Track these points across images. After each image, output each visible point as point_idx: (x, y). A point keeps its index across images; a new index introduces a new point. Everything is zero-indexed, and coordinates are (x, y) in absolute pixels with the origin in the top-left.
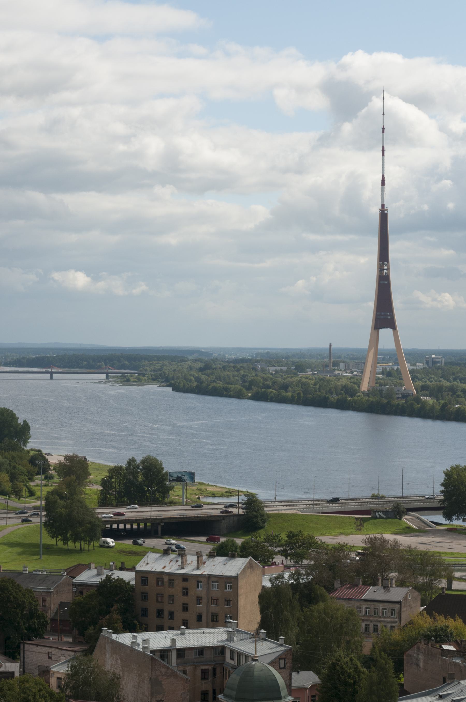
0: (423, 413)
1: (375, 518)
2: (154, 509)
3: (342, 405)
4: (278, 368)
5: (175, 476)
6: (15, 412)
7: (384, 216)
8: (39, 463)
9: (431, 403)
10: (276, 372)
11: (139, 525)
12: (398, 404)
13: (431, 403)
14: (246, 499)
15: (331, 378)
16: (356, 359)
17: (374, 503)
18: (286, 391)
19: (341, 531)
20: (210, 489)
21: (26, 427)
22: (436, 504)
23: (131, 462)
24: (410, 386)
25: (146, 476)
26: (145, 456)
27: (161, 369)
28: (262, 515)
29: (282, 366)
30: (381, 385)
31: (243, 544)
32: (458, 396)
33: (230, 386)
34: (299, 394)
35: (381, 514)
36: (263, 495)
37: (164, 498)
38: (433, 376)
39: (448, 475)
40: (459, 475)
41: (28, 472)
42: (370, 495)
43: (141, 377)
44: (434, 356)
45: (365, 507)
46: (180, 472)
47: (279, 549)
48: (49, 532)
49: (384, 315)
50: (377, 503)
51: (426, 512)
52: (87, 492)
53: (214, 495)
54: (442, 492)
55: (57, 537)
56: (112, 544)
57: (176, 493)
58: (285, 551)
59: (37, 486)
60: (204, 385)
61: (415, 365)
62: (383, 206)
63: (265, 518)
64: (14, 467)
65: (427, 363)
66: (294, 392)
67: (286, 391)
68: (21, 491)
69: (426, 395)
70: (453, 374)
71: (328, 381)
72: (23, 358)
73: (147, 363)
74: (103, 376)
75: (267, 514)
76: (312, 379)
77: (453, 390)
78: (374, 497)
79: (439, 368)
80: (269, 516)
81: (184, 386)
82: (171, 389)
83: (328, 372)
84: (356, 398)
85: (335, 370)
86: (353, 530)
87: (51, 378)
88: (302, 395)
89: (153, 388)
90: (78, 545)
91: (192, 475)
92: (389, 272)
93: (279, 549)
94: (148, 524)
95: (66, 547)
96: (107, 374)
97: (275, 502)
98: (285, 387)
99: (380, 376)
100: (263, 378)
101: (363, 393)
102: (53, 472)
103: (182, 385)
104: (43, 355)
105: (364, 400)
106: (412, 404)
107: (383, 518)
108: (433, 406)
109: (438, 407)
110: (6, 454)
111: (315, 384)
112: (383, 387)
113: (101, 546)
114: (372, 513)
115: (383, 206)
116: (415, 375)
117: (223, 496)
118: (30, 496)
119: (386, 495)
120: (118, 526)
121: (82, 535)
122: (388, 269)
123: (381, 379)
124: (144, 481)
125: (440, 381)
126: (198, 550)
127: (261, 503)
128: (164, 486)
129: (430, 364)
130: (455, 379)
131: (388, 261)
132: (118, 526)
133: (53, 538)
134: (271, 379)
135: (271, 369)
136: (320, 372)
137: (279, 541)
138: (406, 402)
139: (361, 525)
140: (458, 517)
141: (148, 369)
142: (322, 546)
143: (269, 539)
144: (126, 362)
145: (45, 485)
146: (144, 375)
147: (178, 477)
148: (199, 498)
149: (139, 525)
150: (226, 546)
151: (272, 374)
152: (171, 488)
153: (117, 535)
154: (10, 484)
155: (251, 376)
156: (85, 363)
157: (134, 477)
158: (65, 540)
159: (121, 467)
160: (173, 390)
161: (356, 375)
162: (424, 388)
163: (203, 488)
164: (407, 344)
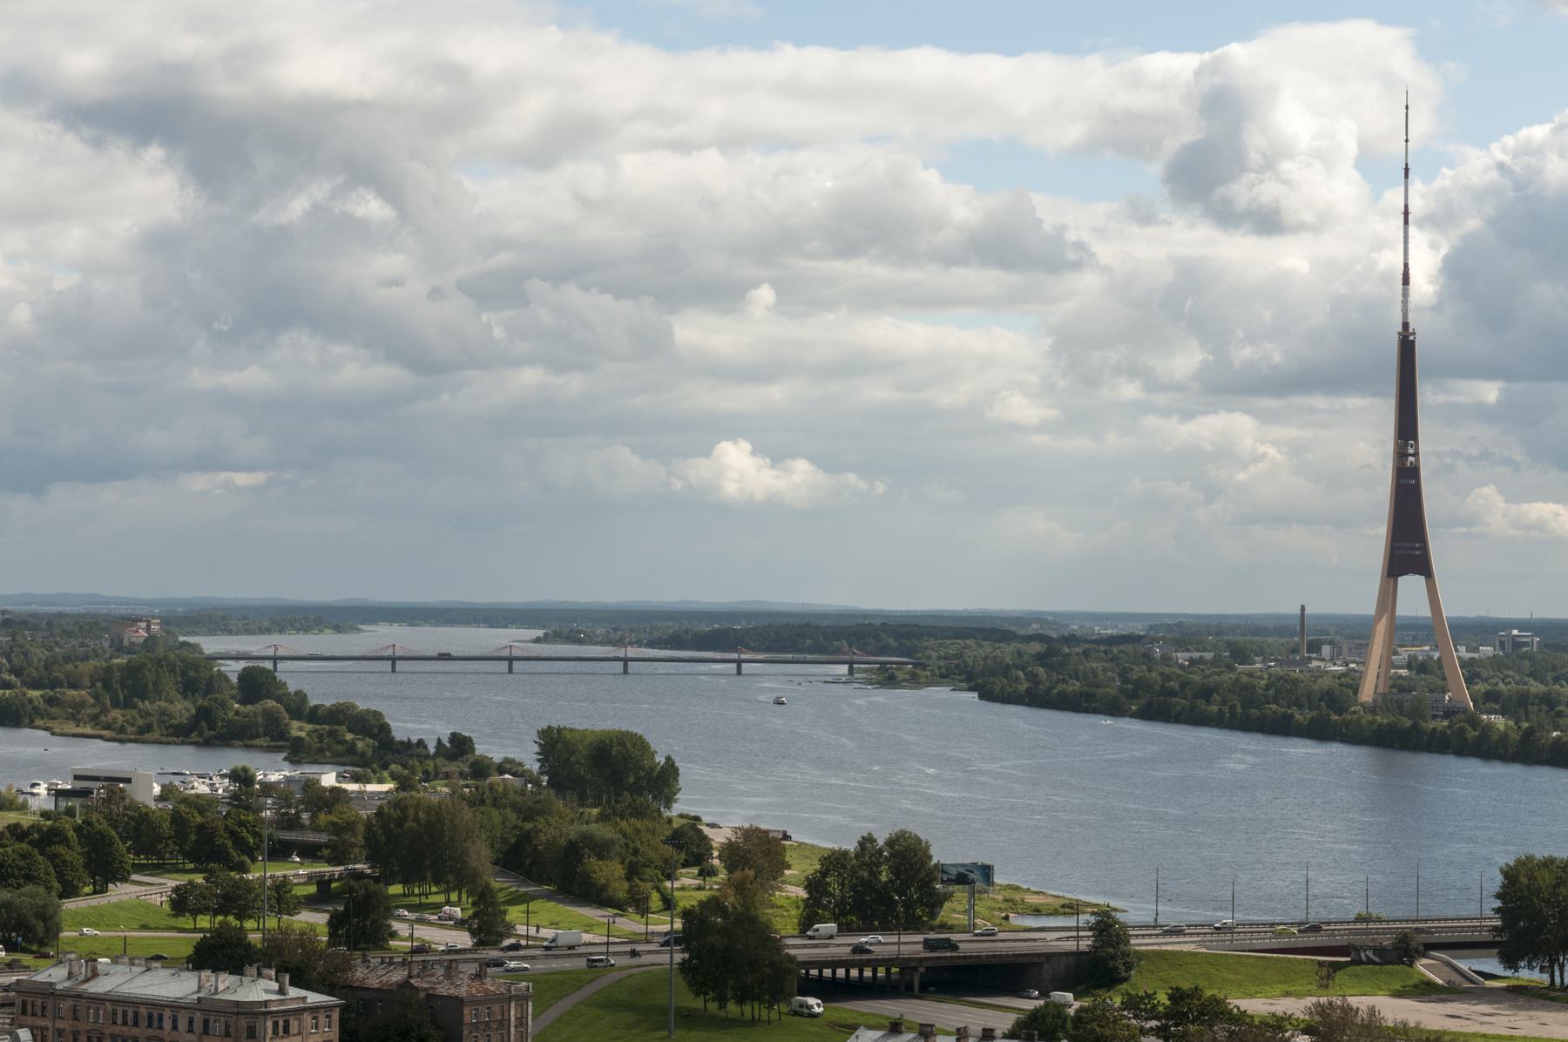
0: (1486, 748)
1: (1357, 962)
2: (904, 938)
3: (1320, 732)
4: (1196, 655)
5: (954, 872)
6: (649, 739)
7: (1407, 347)
8: (689, 844)
9: (1502, 728)
10: (1192, 661)
11: (875, 972)
12: (1434, 729)
13: (1502, 728)
14: (1093, 919)
15: (1301, 676)
16: (1354, 635)
17: (1357, 932)
18: (1208, 702)
19: (1286, 988)
20: (1032, 900)
21: (669, 772)
22: (1486, 936)
23: (866, 841)
24: (1461, 693)
25: (896, 871)
26: (896, 829)
27: (958, 656)
28: (1125, 954)
29: (1205, 650)
30: (1402, 690)
31: (1080, 1010)
32: (1560, 714)
33: (1095, 690)
34: (1233, 707)
35: (1370, 953)
36: (1133, 911)
37: (933, 915)
38: (1511, 673)
39: (1510, 875)
40: (1531, 878)
41: (666, 862)
42: (1352, 916)
43: (919, 672)
44: (1515, 632)
45: (1339, 940)
46: (962, 865)
47: (1154, 1023)
48: (691, 984)
49: (1408, 549)
50: (1366, 932)
51: (1466, 952)
52: (780, 903)
53: (1037, 911)
54: (1497, 910)
55: (706, 994)
56: (817, 1010)
57: (954, 911)
58: (1164, 1028)
59: (683, 889)
60: (1042, 687)
61: (1476, 650)
62: (1406, 325)
63: (1134, 960)
64: (636, 852)
65: (1502, 645)
66: (1224, 703)
67: (1208, 702)
68: (647, 899)
69: (1495, 712)
70: (1554, 668)
71: (1295, 682)
72: (686, 631)
73: (932, 642)
74: (843, 669)
75: (1136, 952)
76: (1261, 678)
77: (1549, 701)
78: (1360, 919)
79: (1527, 656)
80: (1141, 956)
81: (1002, 689)
82: (976, 695)
83: (1296, 663)
84: (1349, 717)
85: (1310, 659)
86: (1313, 987)
87: (739, 672)
88: (1239, 710)
89: (941, 693)
90: (747, 1009)
91: (986, 871)
92: (1417, 460)
93: (1154, 1023)
94: (894, 970)
95: (722, 1013)
96: (851, 663)
97: (1155, 927)
98: (1206, 693)
99: (1404, 672)
100: (1161, 674)
101: (1363, 705)
102: (716, 862)
103: (997, 688)
104: (726, 625)
105: (1364, 722)
106: (1462, 730)
107: (1374, 963)
108: (1505, 735)
109: (1515, 736)
110: (624, 824)
111: (1267, 688)
112: (1405, 696)
113: (796, 1013)
114: (1353, 953)
115: (1406, 325)
116: (1472, 671)
117: (1054, 913)
118: (666, 909)
119: (1384, 915)
120: (834, 972)
121: (756, 991)
122: (1416, 455)
123: (1405, 678)
124: (891, 881)
125: (1526, 683)
126: (961, 1025)
127: (1124, 926)
128: (932, 893)
129: (1509, 648)
130: (1556, 680)
131: (1415, 438)
132: (834, 972)
133: (697, 995)
134: (1179, 676)
135: (1182, 657)
136: (1280, 663)
137: (1154, 1007)
138: (1449, 727)
139: (1329, 977)
140: (1530, 963)
141: (934, 654)
142: (1240, 1018)
143: (1132, 1003)
144: (891, 641)
145: (699, 888)
146: (924, 667)
147: (959, 874)
148: (1007, 918)
149: (875, 972)
150: (1044, 1017)
151: (1182, 667)
152: (948, 897)
153: (831, 990)
154: (626, 885)
155: (1137, 672)
156: (809, 642)
157: (872, 873)
158: (722, 1001)
159: (846, 853)
160: (981, 697)
161: (1353, 670)
162: (1491, 696)
163: (1017, 897)
164: (1455, 607)
